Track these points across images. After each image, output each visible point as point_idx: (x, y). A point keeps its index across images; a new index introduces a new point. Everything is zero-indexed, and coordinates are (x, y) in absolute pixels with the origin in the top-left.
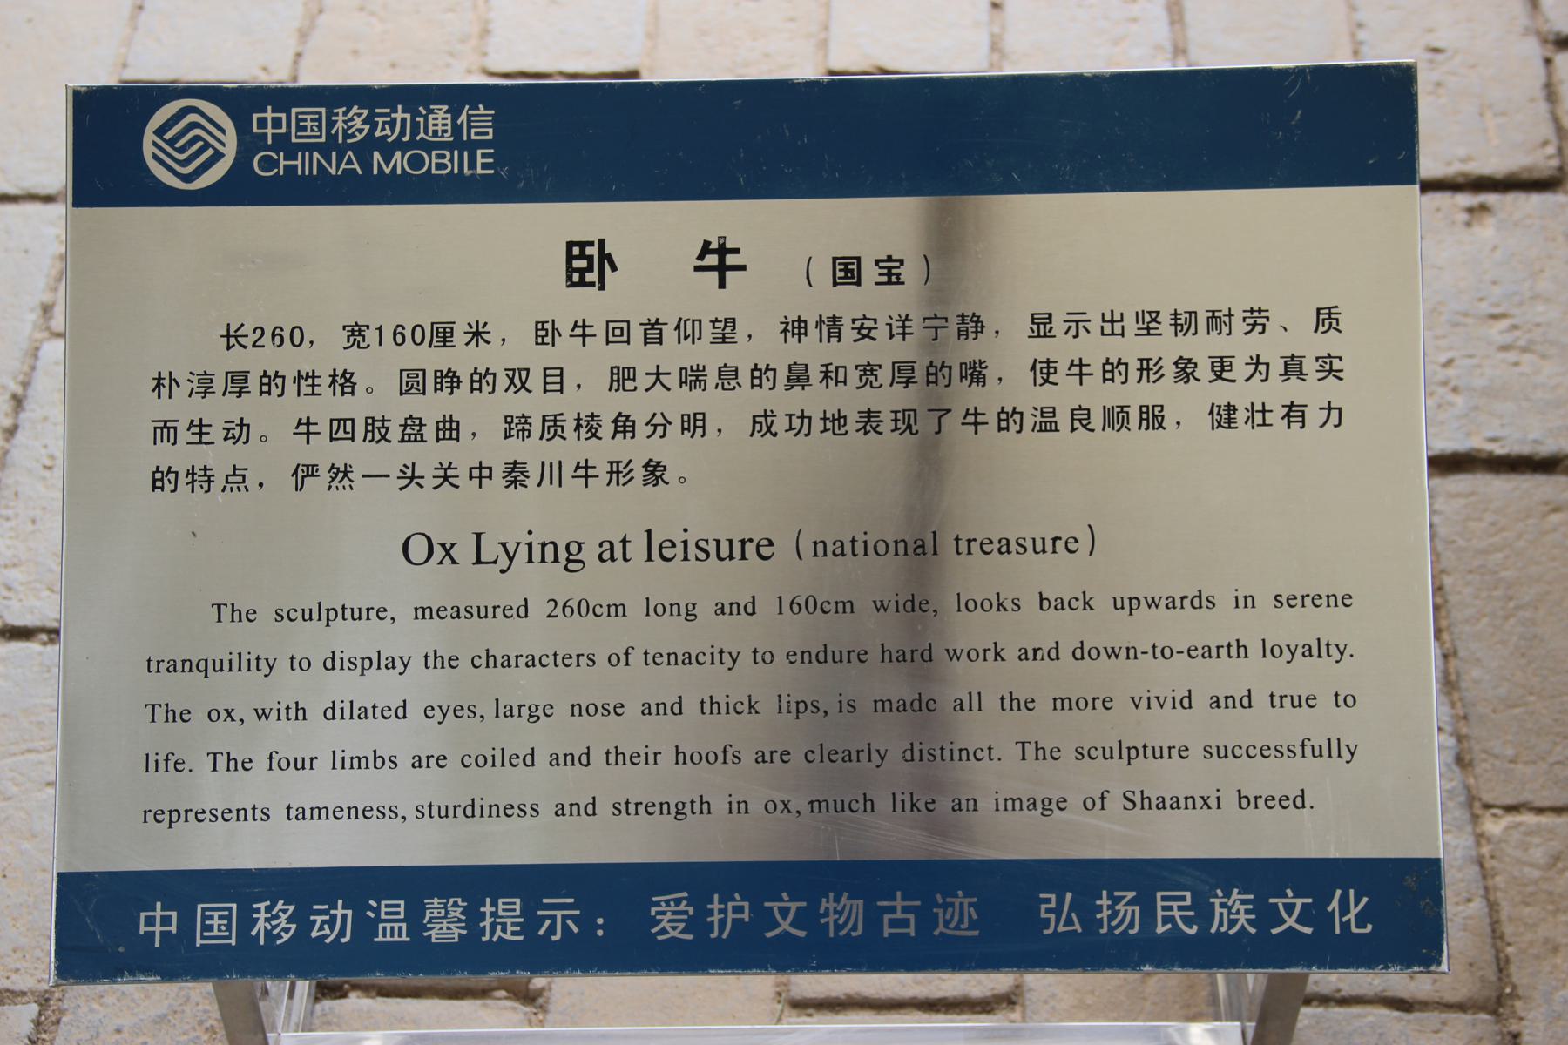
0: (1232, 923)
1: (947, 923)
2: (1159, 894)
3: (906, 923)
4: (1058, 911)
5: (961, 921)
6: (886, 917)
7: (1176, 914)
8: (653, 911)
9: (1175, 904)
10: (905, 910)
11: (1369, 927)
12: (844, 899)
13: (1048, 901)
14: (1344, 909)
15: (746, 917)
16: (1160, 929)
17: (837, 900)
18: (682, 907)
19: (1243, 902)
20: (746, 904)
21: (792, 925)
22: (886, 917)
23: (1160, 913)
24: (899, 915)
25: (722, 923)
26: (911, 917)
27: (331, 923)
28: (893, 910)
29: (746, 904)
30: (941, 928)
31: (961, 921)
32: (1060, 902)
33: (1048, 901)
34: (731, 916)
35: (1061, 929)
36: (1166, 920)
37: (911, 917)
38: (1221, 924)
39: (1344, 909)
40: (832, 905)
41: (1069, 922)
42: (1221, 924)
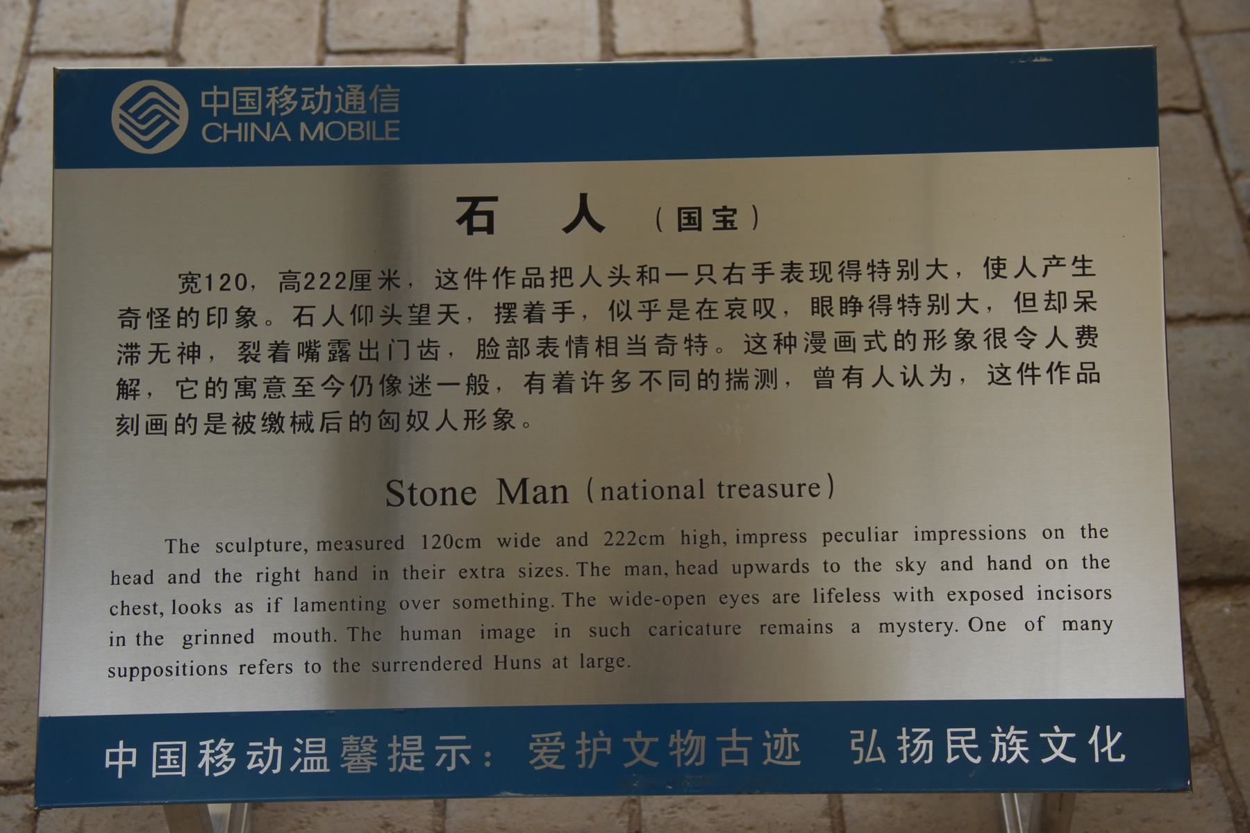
0: (1010, 754)
1: (774, 753)
2: (949, 731)
3: (739, 755)
4: (865, 746)
5: (786, 752)
6: (724, 750)
7: (964, 746)
8: (532, 745)
9: (962, 739)
10: (740, 744)
11: (1123, 757)
12: (689, 736)
13: (858, 736)
14: (1102, 743)
15: (608, 750)
16: (950, 760)
17: (684, 736)
18: (555, 743)
19: (1019, 737)
20: (608, 740)
21: (646, 757)
22: (724, 750)
23: (950, 746)
24: (735, 748)
25: (589, 756)
26: (745, 750)
27: (265, 757)
28: (729, 744)
29: (608, 740)
30: (769, 759)
31: (786, 752)
32: (868, 737)
33: (858, 736)
34: (596, 750)
35: (868, 760)
36: (955, 752)
37: (745, 750)
38: (1001, 755)
39: (1102, 743)
40: (679, 740)
41: (875, 754)
42: (1001, 755)
